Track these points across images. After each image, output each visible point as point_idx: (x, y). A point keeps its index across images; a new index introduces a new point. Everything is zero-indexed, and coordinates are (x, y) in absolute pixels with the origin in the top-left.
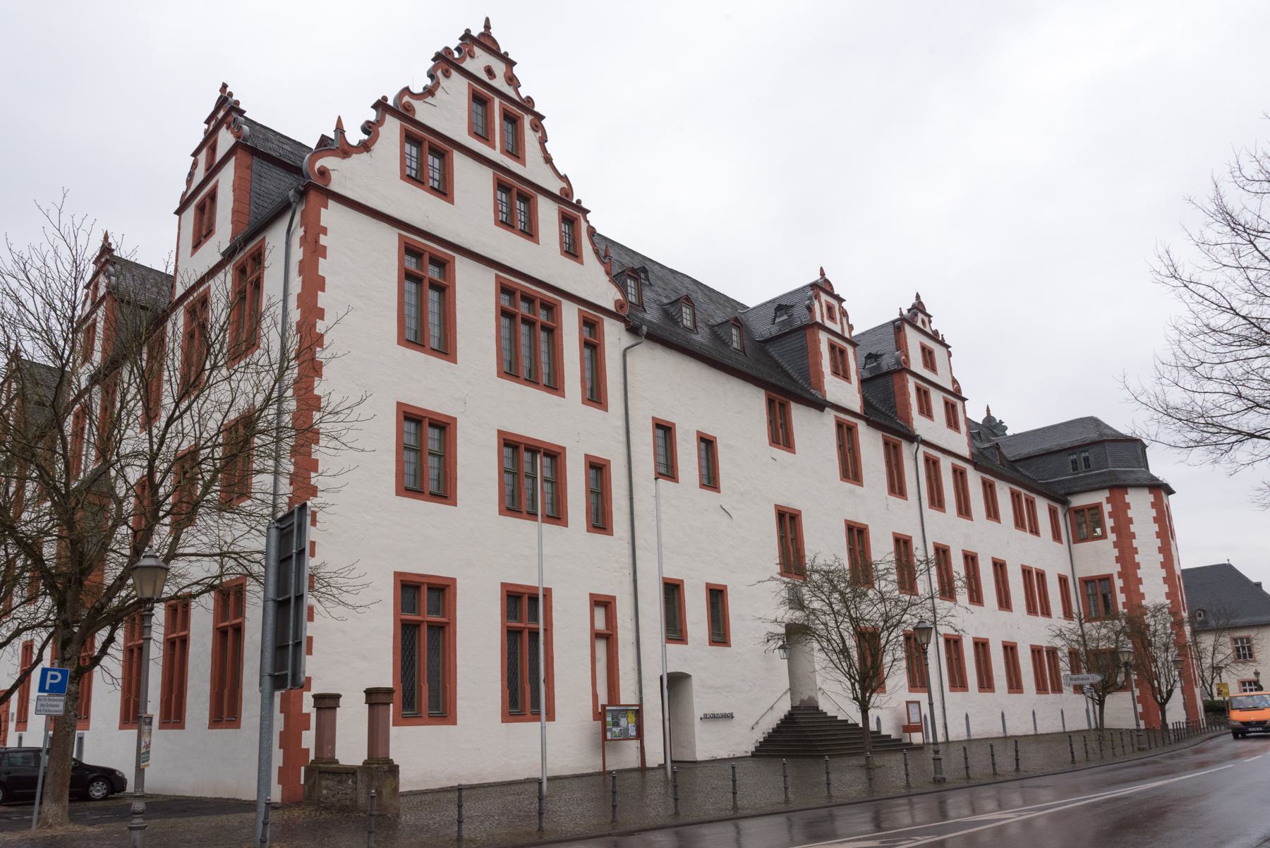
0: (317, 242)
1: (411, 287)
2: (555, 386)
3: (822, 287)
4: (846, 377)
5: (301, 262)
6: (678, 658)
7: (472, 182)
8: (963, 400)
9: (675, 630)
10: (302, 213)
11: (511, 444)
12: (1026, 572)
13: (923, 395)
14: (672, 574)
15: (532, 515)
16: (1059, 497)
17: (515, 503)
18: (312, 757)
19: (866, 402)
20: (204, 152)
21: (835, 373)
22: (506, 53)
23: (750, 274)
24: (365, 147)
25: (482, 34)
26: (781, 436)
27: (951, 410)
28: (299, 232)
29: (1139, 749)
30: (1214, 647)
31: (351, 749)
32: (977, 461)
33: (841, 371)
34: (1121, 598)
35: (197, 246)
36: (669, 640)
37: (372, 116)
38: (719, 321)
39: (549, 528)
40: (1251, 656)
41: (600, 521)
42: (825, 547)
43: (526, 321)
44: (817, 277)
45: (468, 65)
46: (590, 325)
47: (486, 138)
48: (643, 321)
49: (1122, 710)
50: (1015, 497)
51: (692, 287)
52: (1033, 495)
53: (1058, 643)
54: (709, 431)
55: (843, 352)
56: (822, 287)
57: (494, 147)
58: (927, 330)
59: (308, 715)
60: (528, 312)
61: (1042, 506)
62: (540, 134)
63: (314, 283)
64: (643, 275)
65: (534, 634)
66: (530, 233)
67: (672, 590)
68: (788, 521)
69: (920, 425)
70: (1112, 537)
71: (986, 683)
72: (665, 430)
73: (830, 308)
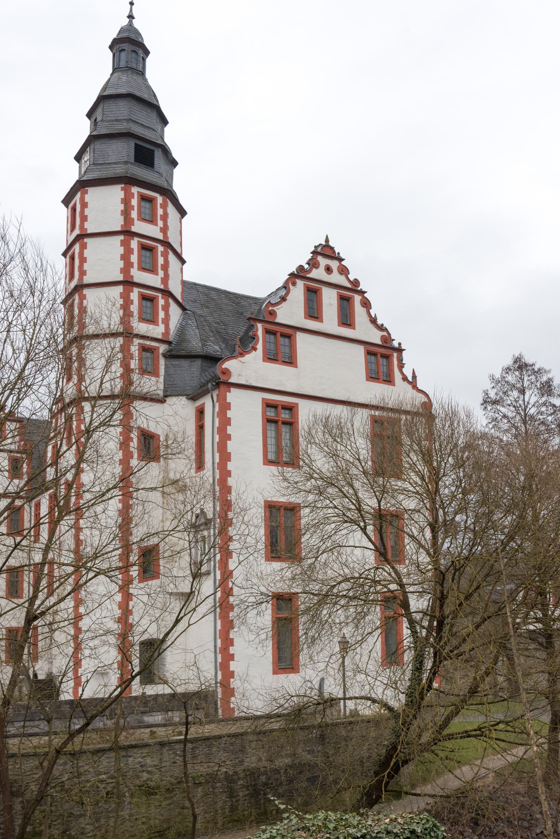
1: (271, 427)
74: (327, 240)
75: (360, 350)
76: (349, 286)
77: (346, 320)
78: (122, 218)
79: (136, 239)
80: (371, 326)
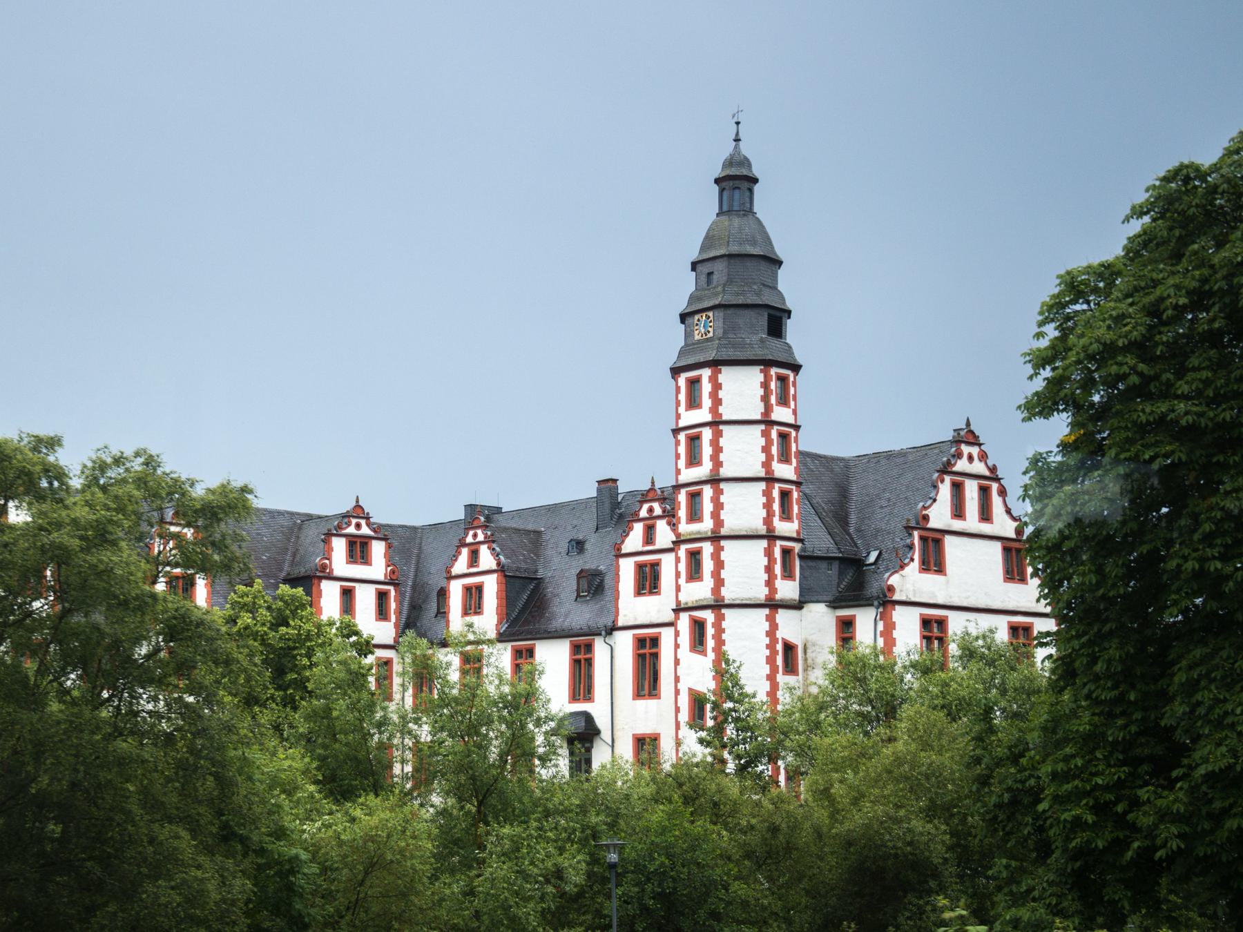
74: (968, 424)
75: (997, 547)
76: (987, 473)
77: (986, 515)
78: (762, 405)
79: (776, 428)
80: (1006, 517)
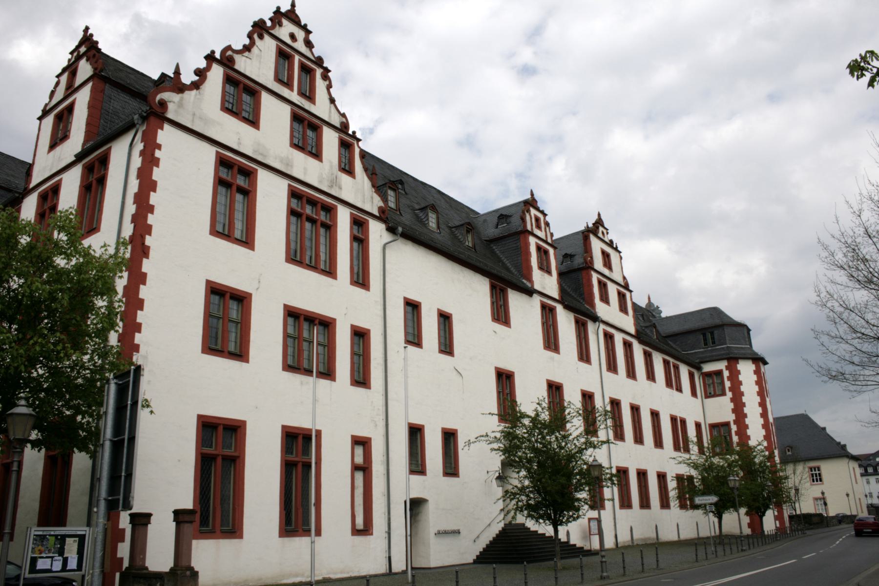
0: (153, 154)
2: (330, 272)
3: (531, 203)
4: (549, 272)
5: (139, 169)
6: (418, 487)
7: (275, 115)
8: (631, 291)
9: (417, 466)
10: (144, 132)
11: (292, 314)
12: (673, 419)
13: (603, 286)
14: (416, 421)
15: (308, 372)
16: (695, 365)
17: (295, 364)
18: (126, 564)
19: (562, 290)
20: (66, 75)
21: (541, 268)
22: (306, 25)
23: (479, 187)
24: (196, 86)
25: (288, 11)
26: (501, 315)
27: (622, 297)
28: (139, 146)
29: (742, 550)
30: (796, 476)
31: (159, 557)
32: (640, 336)
33: (545, 268)
34: (735, 439)
35: (53, 146)
36: (412, 472)
37: (203, 64)
38: (457, 223)
39: (324, 383)
40: (821, 480)
41: (361, 379)
42: (530, 398)
43: (312, 221)
44: (529, 196)
45: (277, 32)
46: (359, 224)
47: (288, 85)
48: (399, 224)
49: (735, 521)
50: (666, 363)
51: (437, 196)
52: (678, 363)
53: (694, 473)
54: (447, 309)
55: (546, 252)
56: (531, 203)
57: (292, 90)
58: (606, 239)
59: (124, 530)
60: (310, 211)
61: (684, 370)
62: (327, 83)
63: (147, 185)
64: (400, 186)
65: (308, 466)
66: (317, 155)
67: (416, 433)
68: (505, 378)
69: (601, 309)
70: (729, 395)
71: (645, 504)
72: (413, 307)
73: (537, 220)
